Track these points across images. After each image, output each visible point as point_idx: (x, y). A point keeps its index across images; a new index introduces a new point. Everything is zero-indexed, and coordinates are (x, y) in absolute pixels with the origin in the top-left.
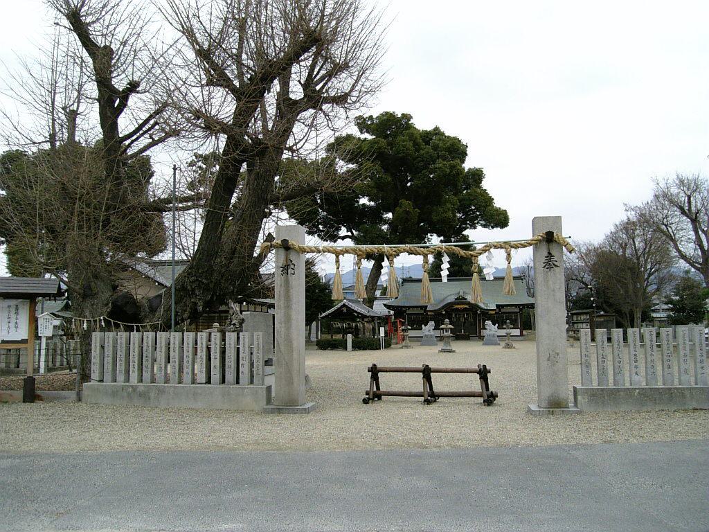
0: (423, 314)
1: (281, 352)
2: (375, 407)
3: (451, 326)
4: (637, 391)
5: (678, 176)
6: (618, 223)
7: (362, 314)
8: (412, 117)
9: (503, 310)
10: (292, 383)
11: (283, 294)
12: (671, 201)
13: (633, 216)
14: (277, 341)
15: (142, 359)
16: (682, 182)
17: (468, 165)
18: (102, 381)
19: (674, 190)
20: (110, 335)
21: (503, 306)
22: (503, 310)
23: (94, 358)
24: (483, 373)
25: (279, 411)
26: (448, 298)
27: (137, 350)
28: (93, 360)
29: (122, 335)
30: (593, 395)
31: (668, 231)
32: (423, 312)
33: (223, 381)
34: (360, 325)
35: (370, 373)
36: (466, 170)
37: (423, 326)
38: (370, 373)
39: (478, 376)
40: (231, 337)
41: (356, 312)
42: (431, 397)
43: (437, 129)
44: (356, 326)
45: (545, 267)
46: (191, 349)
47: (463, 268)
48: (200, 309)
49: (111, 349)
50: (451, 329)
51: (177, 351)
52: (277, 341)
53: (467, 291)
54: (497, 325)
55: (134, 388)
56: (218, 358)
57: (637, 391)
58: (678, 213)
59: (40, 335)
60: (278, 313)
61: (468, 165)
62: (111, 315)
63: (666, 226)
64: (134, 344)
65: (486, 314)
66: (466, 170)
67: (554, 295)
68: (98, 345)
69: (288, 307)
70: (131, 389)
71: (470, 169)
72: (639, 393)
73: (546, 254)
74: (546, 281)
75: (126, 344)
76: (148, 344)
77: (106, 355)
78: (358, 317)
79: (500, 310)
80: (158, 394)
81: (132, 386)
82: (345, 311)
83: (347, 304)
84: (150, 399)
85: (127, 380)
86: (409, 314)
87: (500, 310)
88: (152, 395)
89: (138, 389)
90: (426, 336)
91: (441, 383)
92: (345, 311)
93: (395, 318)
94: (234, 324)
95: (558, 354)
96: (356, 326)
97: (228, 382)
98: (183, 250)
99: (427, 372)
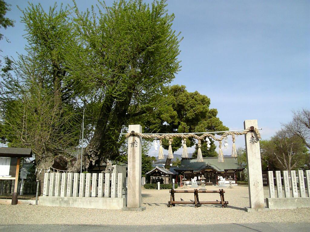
0: (191, 174)
1: (130, 182)
2: (173, 208)
3: (205, 178)
4: (296, 200)
5: (304, 110)
6: (277, 132)
7: (164, 173)
8: (186, 87)
9: (227, 172)
10: (135, 197)
11: (131, 156)
12: (301, 121)
13: (284, 128)
14: (129, 177)
15: (67, 185)
16: (305, 113)
17: (211, 108)
18: (47, 196)
19: (302, 117)
20: (52, 174)
21: (227, 170)
22: (227, 172)
23: (45, 185)
24: (222, 193)
25: (129, 209)
26: (203, 166)
27: (64, 182)
28: (44, 186)
29: (58, 174)
30: (276, 202)
31: (300, 134)
32: (191, 173)
33: (103, 195)
34: (164, 178)
35: (170, 193)
36: (210, 110)
37: (192, 179)
38: (170, 193)
39: (219, 194)
40: (107, 175)
41: (162, 172)
42: (198, 204)
43: (196, 92)
44: (162, 179)
45: (250, 142)
46: (89, 181)
47: (209, 153)
48: (93, 164)
49: (53, 180)
50: (205, 179)
51: (83, 182)
52: (129, 177)
53: (211, 164)
54: (225, 178)
55: (62, 199)
56: (102, 185)
57: (296, 200)
58: (305, 126)
59: (21, 178)
60: (129, 166)
61: (211, 108)
62: (53, 166)
63: (300, 132)
64: (63, 178)
65: (220, 174)
66: (210, 110)
67: (255, 155)
68: (47, 179)
69: (134, 161)
70: (61, 199)
71: (211, 109)
72: (297, 201)
73: (251, 137)
74: (251, 149)
75: (60, 179)
76: (69, 178)
77: (50, 183)
78: (162, 174)
79: (226, 172)
80: (73, 202)
81: (61, 198)
82: (157, 171)
83: (158, 168)
84: (69, 204)
85: (59, 195)
86: (185, 174)
87: (226, 172)
88: (70, 202)
89: (64, 199)
90: (193, 183)
91: (202, 198)
92: (157, 171)
93: (192, 141)
94: (109, 170)
95: (258, 183)
96: (162, 179)
97: (106, 196)
98: (98, 61)
99: (196, 193)
